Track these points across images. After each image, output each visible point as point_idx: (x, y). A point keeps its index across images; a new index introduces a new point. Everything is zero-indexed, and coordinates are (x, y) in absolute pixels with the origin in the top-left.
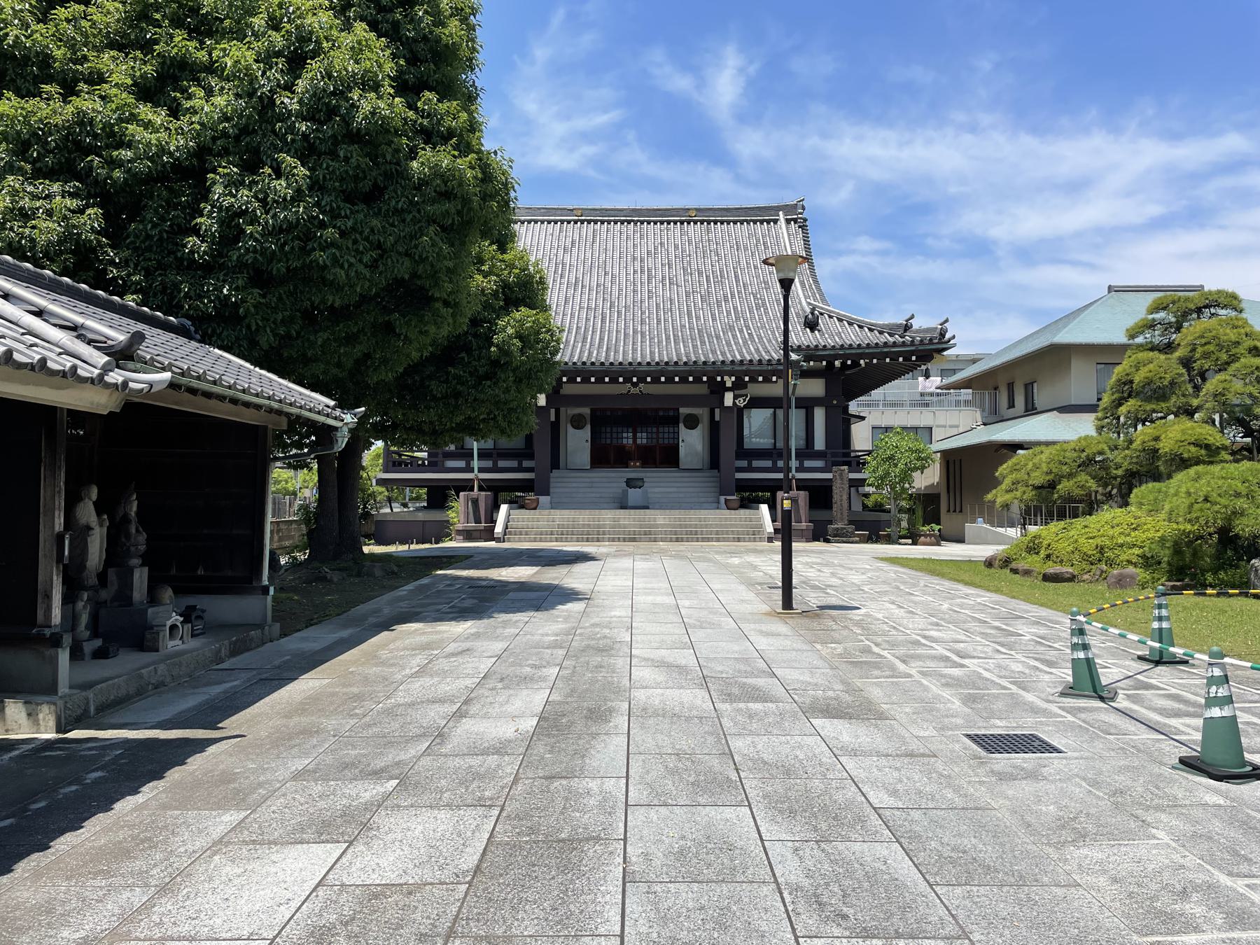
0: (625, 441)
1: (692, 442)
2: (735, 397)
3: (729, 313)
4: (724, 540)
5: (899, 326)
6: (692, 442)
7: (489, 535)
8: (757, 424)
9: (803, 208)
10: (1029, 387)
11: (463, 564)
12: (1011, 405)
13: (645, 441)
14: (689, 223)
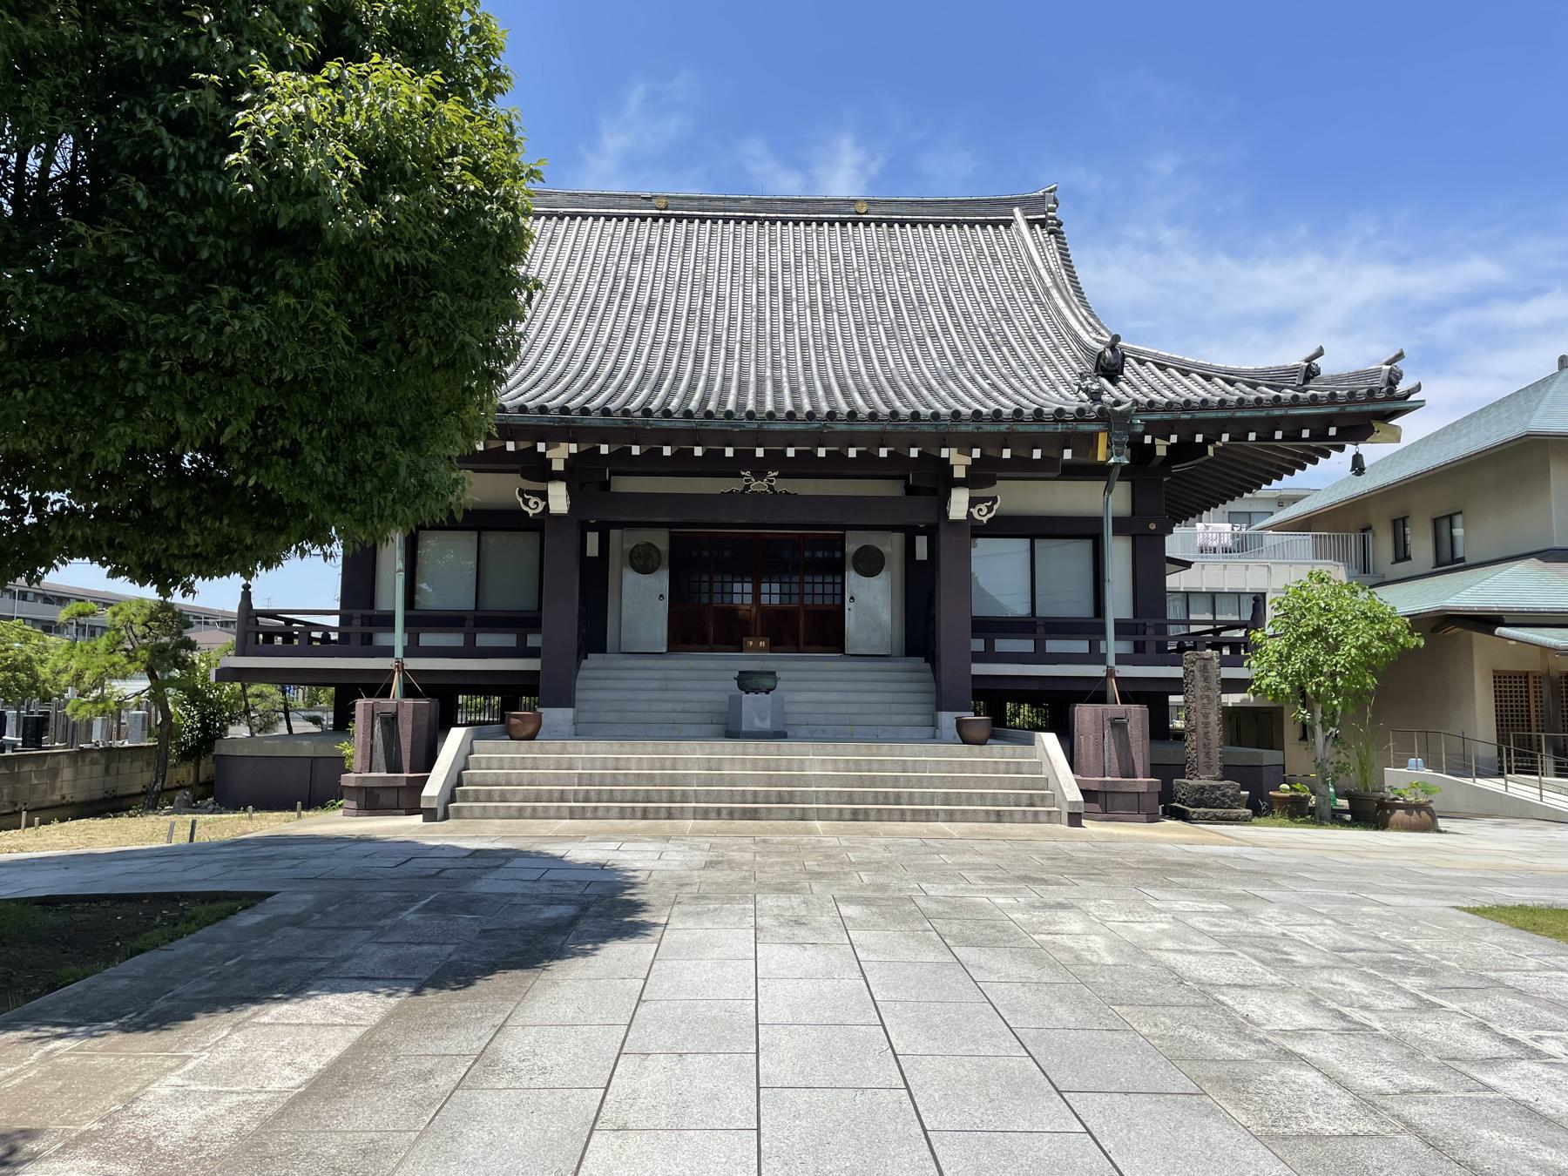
0: (737, 600)
1: (871, 603)
2: (973, 502)
3: (942, 355)
4: (965, 817)
5: (1293, 371)
6: (871, 603)
7: (407, 800)
8: (1000, 576)
9: (1055, 201)
10: (1441, 525)
11: (119, 977)
12: (1402, 555)
13: (776, 600)
14: (855, 224)
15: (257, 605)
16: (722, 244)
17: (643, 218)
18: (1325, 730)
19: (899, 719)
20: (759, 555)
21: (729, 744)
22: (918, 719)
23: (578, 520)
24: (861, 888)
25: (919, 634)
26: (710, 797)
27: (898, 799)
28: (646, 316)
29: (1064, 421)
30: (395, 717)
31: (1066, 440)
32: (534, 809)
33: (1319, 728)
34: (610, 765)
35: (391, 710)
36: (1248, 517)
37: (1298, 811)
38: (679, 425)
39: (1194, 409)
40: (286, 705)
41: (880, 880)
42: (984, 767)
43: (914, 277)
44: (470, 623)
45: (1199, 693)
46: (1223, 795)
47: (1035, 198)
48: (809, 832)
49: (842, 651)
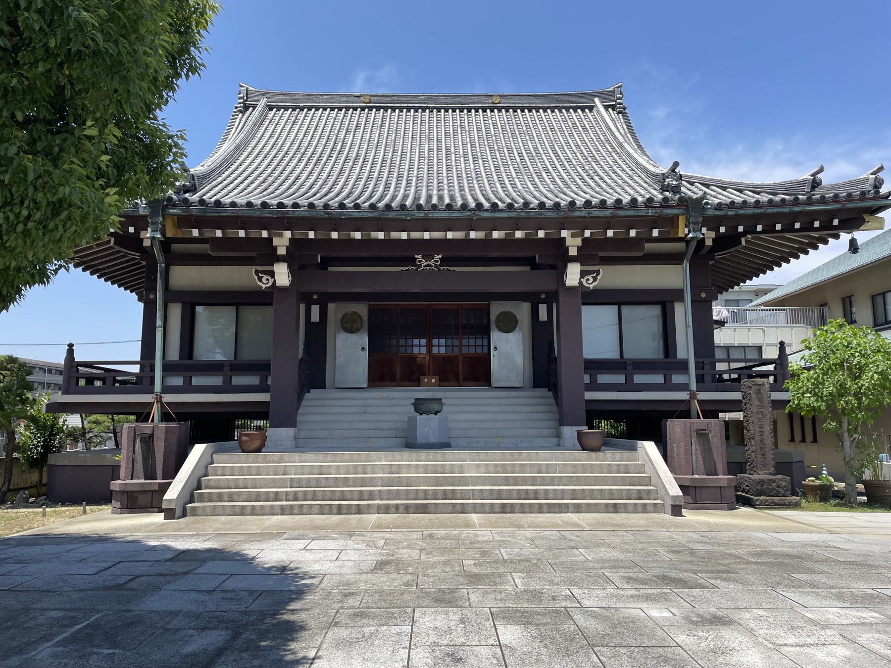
0: (416, 350)
1: (509, 351)
2: (583, 274)
3: (554, 182)
4: (590, 509)
5: (802, 183)
6: (509, 351)
8: (597, 333)
13: (443, 350)
14: (492, 110)
15: (78, 358)
16: (407, 123)
17: (355, 109)
18: (851, 436)
19: (533, 432)
20: (430, 323)
21: (406, 453)
22: (545, 432)
23: (300, 293)
24: (517, 597)
25: (545, 371)
26: (391, 495)
27: (536, 495)
28: (354, 163)
29: (652, 207)
30: (151, 436)
31: (654, 222)
32: (253, 507)
33: (846, 435)
34: (315, 471)
35: (149, 431)
36: (737, 302)
37: (826, 496)
38: (366, 215)
39: (737, 207)
40: (114, 429)
41: (534, 585)
42: (601, 469)
43: (532, 139)
44: (227, 368)
45: (755, 410)
46: (778, 486)
47: (608, 92)
48: (468, 525)
49: (490, 385)
